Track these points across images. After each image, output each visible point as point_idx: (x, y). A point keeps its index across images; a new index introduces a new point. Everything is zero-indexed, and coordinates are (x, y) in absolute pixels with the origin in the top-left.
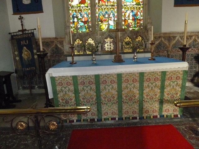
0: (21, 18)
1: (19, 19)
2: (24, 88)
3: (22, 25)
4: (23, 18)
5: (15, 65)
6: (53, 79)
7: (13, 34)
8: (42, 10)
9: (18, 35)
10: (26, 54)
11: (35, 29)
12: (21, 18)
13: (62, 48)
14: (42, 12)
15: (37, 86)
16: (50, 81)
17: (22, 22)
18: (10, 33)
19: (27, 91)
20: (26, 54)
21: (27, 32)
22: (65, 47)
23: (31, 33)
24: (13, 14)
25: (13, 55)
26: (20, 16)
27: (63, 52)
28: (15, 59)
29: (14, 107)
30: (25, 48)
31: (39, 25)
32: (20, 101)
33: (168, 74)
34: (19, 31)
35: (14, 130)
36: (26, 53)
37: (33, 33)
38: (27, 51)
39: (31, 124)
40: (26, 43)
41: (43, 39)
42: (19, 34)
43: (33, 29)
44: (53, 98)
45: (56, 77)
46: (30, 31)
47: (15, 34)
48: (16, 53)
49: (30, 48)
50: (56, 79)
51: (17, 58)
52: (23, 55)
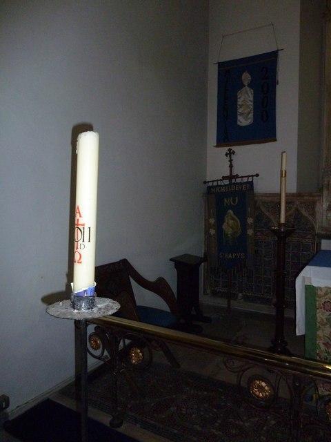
0: (230, 154)
1: (226, 155)
2: (215, 294)
3: (231, 166)
4: (234, 153)
5: (205, 244)
6: (310, 291)
7: (210, 184)
8: (275, 135)
9: (221, 186)
10: (230, 224)
11: (257, 175)
12: (230, 154)
13: (310, 218)
14: (276, 140)
15: (240, 294)
16: (304, 294)
17: (231, 161)
18: (205, 182)
19: (222, 302)
20: (230, 224)
21: (238, 180)
22: (318, 216)
23: (248, 182)
24: (217, 146)
25: (205, 225)
26: (230, 150)
27: (313, 228)
28: (207, 232)
29: (198, 331)
30: (231, 212)
31: (284, 168)
32: (208, 320)
33: (322, 294)
34: (224, 178)
35: (241, 394)
36: (231, 222)
37: (251, 184)
38: (233, 219)
39: (284, 393)
40: (234, 201)
41: (287, 195)
42: (223, 184)
43: (252, 176)
44: (304, 335)
45: (320, 288)
46: (245, 180)
47: (215, 184)
48: (212, 221)
49: (241, 213)
50: (319, 292)
51: (213, 232)
52: (225, 226)
